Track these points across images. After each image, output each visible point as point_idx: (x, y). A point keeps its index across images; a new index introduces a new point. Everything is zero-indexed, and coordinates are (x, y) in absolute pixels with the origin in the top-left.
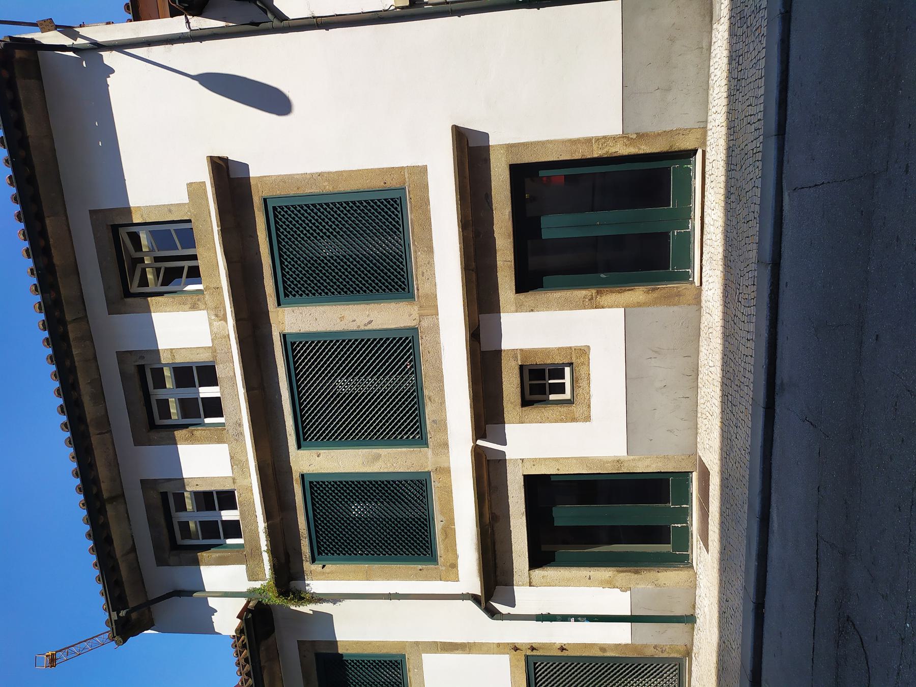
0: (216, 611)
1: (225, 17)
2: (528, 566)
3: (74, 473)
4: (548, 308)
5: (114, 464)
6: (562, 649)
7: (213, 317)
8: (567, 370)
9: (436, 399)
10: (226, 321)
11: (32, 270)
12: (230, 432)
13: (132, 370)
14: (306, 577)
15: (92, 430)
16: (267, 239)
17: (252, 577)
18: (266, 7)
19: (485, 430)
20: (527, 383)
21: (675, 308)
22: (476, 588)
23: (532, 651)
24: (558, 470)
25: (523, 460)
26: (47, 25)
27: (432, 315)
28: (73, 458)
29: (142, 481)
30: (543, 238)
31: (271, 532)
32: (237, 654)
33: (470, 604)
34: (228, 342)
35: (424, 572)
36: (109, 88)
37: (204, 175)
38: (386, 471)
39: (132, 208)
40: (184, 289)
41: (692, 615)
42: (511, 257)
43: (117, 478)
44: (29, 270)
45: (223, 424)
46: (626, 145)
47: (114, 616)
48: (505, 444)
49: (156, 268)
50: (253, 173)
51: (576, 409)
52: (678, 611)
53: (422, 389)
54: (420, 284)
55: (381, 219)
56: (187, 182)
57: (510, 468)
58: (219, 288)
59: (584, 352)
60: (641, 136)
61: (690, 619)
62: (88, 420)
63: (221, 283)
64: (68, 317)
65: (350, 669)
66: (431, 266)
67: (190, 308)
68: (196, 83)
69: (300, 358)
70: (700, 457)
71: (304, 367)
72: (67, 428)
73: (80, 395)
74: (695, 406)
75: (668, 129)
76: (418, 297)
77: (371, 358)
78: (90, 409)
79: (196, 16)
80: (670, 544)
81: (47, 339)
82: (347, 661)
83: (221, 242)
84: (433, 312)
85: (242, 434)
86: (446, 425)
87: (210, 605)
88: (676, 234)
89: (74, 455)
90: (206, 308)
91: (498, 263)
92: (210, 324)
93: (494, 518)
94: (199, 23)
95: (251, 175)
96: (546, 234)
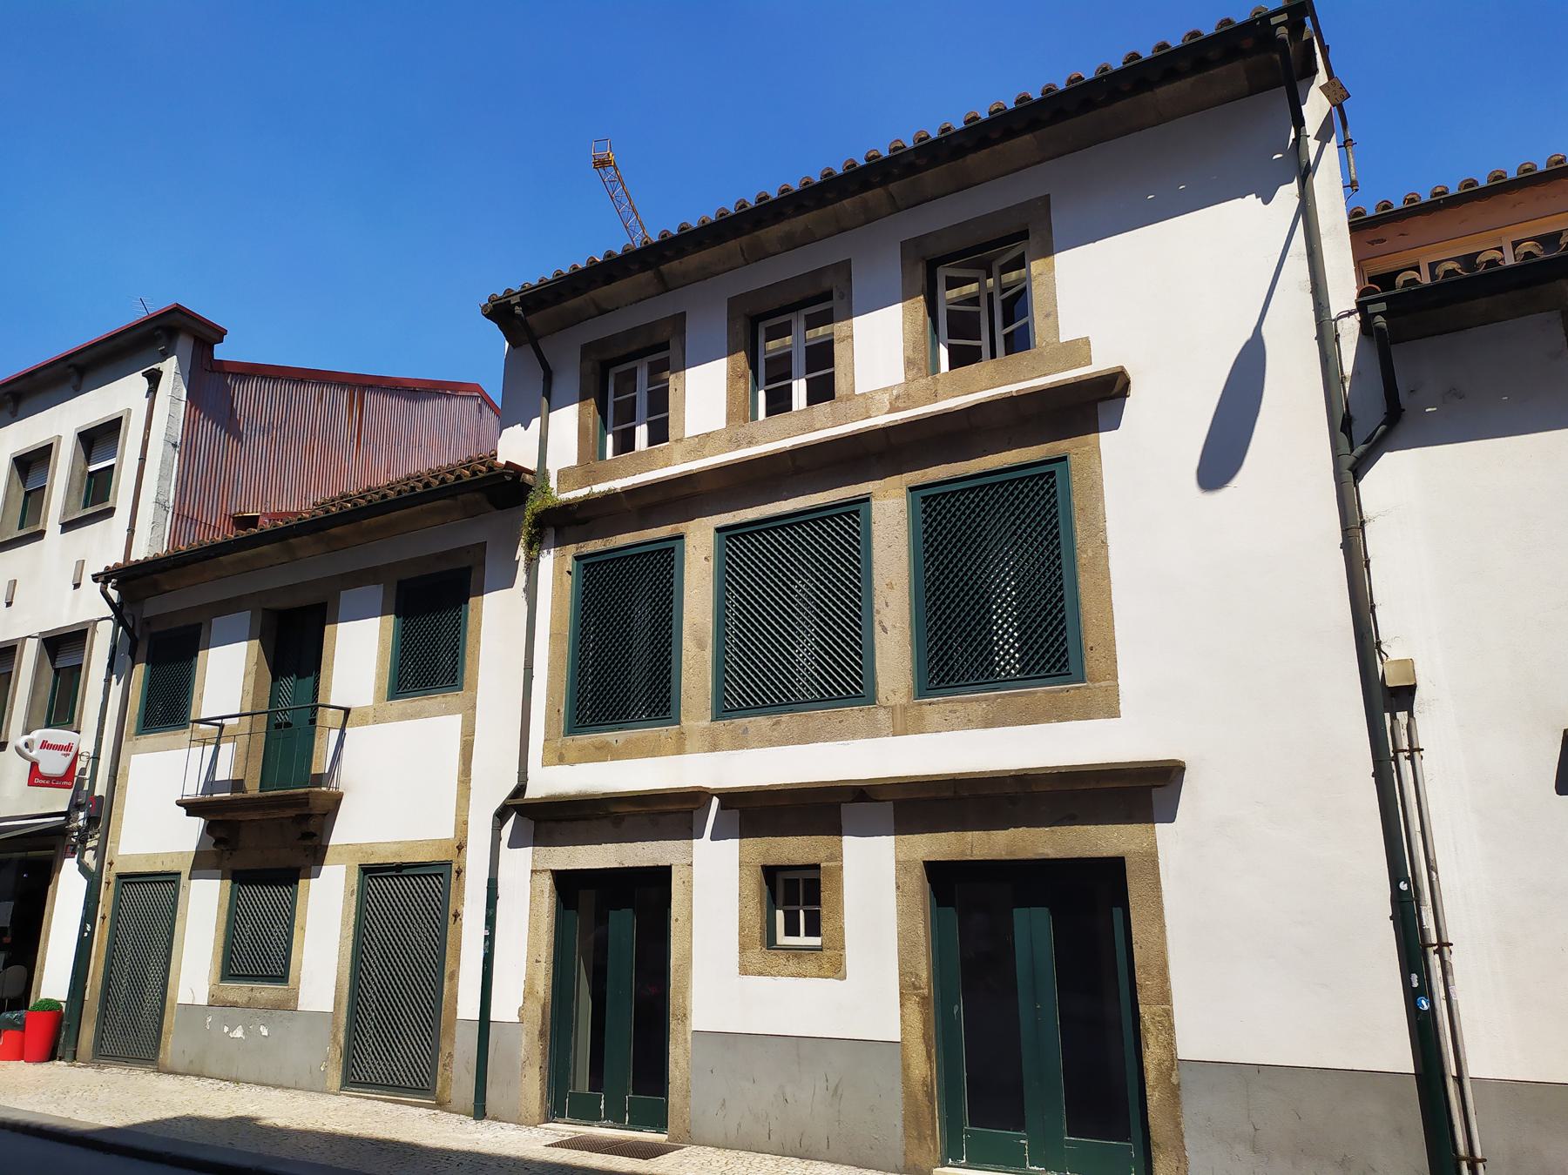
0: (526, 429)
1: (1359, 373)
2: (556, 868)
3: (684, 226)
4: (901, 914)
5: (705, 274)
6: (456, 915)
7: (895, 392)
8: (815, 941)
9: (775, 733)
10: (889, 412)
11: (948, 129)
12: (742, 430)
13: (826, 283)
14: (558, 549)
15: (745, 239)
16: (1006, 466)
17: (563, 474)
18: (1376, 441)
19: (731, 808)
20: (800, 876)
21: (900, 1130)
22: (534, 792)
23: (456, 872)
24: (677, 920)
25: (691, 865)
26: (1337, 93)
27: (893, 726)
28: (703, 222)
29: (685, 313)
30: (1015, 910)
31: (610, 498)
32: (481, 458)
33: (513, 783)
34: (861, 418)
35: (555, 715)
36: (1240, 199)
37: (1100, 364)
38: (684, 658)
39: (1051, 258)
40: (941, 345)
41: (486, 1115)
42: (978, 854)
43: (688, 280)
44: (948, 125)
45: (755, 417)
46: (1159, 1065)
47: (515, 299)
48: (712, 839)
49: (978, 297)
50: (1105, 438)
51: (757, 954)
52: (492, 1094)
53: (791, 711)
54: (937, 707)
55: (1037, 643)
56: (1090, 336)
57: (680, 844)
58: (935, 398)
59: (837, 970)
60: (1174, 1092)
61: (480, 1111)
62: (756, 233)
63: (942, 400)
64: (893, 187)
65: (425, 620)
66: (966, 724)
67: (908, 357)
68: (1249, 335)
69: (813, 529)
70: (682, 1148)
71: (761, 543)
72: (740, 208)
73: (789, 218)
74: (757, 1150)
75: (1186, 1141)
76: (920, 704)
77: (835, 632)
78: (772, 233)
79: (1361, 325)
80: (589, 1091)
81: (854, 165)
82: (460, 610)
83: (995, 398)
84: (898, 728)
85: (738, 447)
86: (742, 747)
87: (1281, 189)
88: (1022, 1141)
89: (708, 222)
90: (907, 381)
91: (970, 833)
92: (885, 390)
93: (618, 820)
94: (1349, 332)
95: (1102, 435)
96: (1020, 915)
